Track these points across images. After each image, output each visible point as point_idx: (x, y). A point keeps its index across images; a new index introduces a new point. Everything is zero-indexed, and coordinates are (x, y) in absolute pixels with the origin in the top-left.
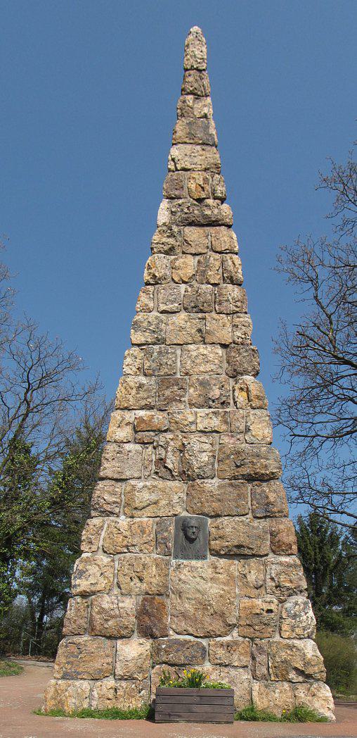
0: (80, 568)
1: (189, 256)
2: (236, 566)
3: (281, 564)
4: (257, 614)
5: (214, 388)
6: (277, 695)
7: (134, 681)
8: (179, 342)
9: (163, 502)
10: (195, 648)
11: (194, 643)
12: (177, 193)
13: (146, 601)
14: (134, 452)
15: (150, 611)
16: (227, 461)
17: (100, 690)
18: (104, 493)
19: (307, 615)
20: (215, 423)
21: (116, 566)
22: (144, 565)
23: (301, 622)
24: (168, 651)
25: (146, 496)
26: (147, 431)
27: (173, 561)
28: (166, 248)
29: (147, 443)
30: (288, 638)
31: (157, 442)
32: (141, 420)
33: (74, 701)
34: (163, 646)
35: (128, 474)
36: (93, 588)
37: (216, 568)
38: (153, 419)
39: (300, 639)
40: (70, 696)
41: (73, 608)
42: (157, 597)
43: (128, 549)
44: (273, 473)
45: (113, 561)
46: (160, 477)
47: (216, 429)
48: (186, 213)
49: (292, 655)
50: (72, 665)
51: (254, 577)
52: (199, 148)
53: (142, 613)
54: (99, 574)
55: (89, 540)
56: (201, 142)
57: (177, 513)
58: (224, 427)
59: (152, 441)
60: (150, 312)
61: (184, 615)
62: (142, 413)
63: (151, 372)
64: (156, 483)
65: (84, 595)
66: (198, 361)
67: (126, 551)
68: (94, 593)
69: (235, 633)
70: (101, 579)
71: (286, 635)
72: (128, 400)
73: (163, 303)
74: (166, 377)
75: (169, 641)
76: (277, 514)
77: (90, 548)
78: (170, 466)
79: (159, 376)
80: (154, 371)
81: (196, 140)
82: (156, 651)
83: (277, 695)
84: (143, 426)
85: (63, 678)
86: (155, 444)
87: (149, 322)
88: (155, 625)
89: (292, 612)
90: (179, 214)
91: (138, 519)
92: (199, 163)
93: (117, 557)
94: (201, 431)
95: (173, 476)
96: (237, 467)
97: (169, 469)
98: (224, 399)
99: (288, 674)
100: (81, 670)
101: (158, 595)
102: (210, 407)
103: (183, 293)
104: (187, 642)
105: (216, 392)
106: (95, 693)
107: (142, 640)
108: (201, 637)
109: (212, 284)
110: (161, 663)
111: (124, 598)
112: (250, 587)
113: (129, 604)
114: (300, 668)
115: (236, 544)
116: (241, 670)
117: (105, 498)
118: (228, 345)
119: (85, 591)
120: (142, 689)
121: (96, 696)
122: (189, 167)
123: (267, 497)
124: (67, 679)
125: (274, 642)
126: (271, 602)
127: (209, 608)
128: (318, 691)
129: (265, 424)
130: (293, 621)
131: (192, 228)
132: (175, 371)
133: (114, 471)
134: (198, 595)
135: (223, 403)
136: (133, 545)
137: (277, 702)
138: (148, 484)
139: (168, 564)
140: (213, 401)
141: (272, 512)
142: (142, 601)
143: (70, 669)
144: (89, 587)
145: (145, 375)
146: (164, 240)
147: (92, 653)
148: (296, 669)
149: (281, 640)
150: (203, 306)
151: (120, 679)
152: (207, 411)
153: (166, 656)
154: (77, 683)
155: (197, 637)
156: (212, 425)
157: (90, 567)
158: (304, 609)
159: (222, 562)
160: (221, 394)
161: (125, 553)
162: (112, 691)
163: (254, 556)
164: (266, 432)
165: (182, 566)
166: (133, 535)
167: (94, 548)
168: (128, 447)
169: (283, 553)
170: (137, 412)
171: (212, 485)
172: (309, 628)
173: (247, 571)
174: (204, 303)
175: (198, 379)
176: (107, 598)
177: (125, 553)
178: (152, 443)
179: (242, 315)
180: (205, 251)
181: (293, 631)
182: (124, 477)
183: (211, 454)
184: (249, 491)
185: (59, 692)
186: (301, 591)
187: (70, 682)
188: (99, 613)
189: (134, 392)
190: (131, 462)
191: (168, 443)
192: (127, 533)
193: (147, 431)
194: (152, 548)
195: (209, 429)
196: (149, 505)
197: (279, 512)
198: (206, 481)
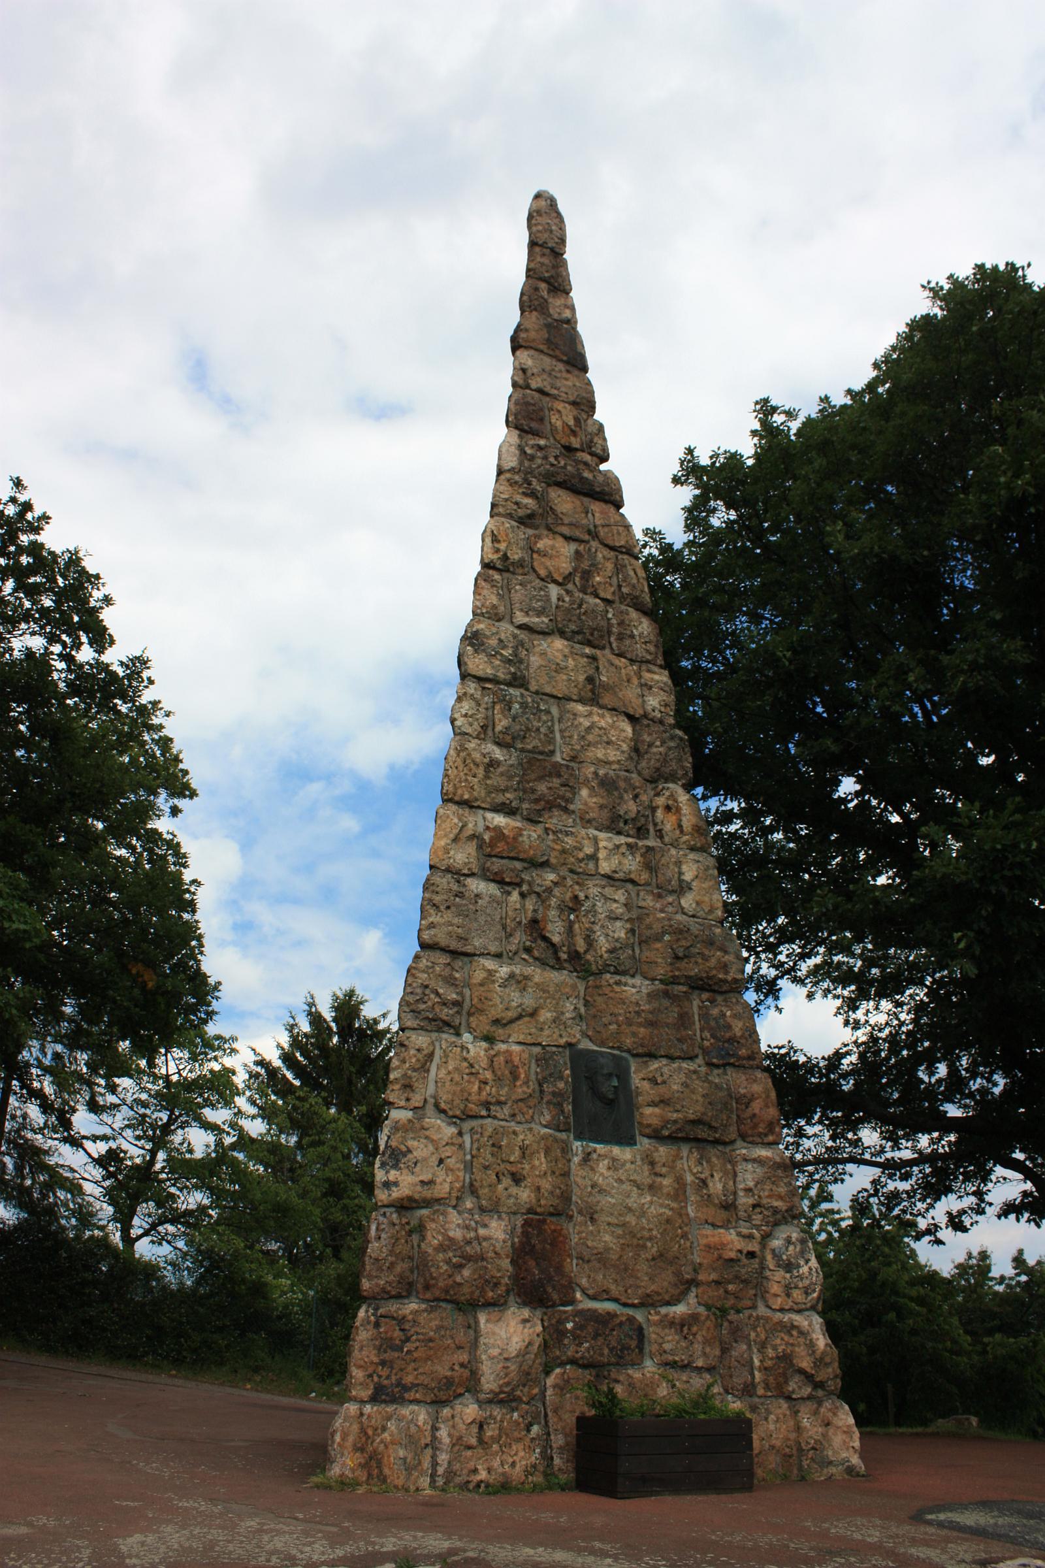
1: (561, 539)
2: (688, 1162)
3: (758, 1161)
4: (732, 1260)
7: (514, 1404)
8: (555, 693)
9: (546, 1015)
10: (626, 1328)
11: (624, 1319)
12: (534, 425)
13: (530, 1225)
14: (487, 899)
15: (538, 1247)
16: (658, 945)
17: (453, 1427)
19: (810, 1264)
20: (631, 864)
21: (468, 1145)
22: (523, 1149)
23: (801, 1277)
24: (578, 1336)
26: (508, 858)
27: (577, 1145)
28: (521, 512)
29: (509, 884)
30: (781, 1310)
31: (530, 884)
33: (401, 1453)
34: (569, 1325)
36: (427, 1193)
38: (521, 835)
40: (393, 1443)
41: (383, 1236)
42: (549, 1219)
43: (488, 1110)
45: (460, 1134)
46: (536, 959)
47: (633, 876)
48: (552, 465)
49: (792, 1345)
50: (392, 1368)
51: (719, 1186)
52: (560, 366)
53: (523, 1252)
54: (434, 1160)
55: (406, 1082)
56: (565, 358)
58: (644, 876)
59: (518, 880)
60: (499, 620)
61: (601, 1258)
62: (499, 820)
63: (508, 739)
64: (529, 970)
65: (405, 1206)
66: (590, 737)
67: (484, 1113)
68: (427, 1203)
69: (692, 1298)
70: (441, 1175)
71: (777, 1303)
72: (472, 788)
73: (521, 610)
74: (541, 757)
77: (408, 1100)
79: (522, 750)
80: (514, 738)
81: (558, 353)
82: (554, 1335)
84: (501, 847)
85: (374, 1399)
86: (525, 888)
87: (501, 641)
88: (550, 1279)
89: (784, 1257)
90: (539, 461)
91: (503, 1047)
92: (563, 389)
93: (467, 1126)
95: (558, 959)
96: (677, 958)
97: (553, 945)
99: (786, 1382)
101: (551, 1214)
102: (619, 833)
103: (554, 599)
104: (611, 1315)
105: (630, 807)
106: (443, 1433)
107: (526, 1313)
108: (633, 1306)
109: (603, 600)
110: (562, 1364)
111: (486, 1219)
112: (715, 1205)
113: (497, 1231)
114: (809, 1370)
115: (692, 1117)
117: (441, 991)
120: (531, 1424)
121: (447, 1440)
122: (548, 389)
124: (385, 1402)
125: (758, 1318)
126: (750, 1237)
127: (649, 1244)
128: (835, 1414)
130: (788, 1275)
131: (561, 492)
132: (551, 748)
133: (449, 934)
134: (631, 1219)
136: (499, 1103)
139: (566, 1149)
140: (626, 822)
141: (740, 1058)
142: (523, 1226)
143: (388, 1377)
144: (419, 1188)
145: (498, 744)
146: (518, 498)
147: (431, 1340)
148: (801, 1371)
149: (769, 1313)
150: (592, 634)
151: (490, 1401)
153: (572, 1348)
154: (406, 1411)
155: (625, 1305)
156: (626, 868)
157: (416, 1143)
158: (802, 1252)
159: (663, 1152)
161: (482, 1117)
162: (475, 1429)
163: (717, 1142)
165: (595, 1156)
166: (498, 1079)
167: (417, 1100)
169: (759, 1140)
170: (489, 815)
172: (814, 1291)
173: (706, 1174)
174: (594, 629)
175: (596, 774)
176: (454, 1217)
177: (482, 1117)
178: (519, 885)
180: (587, 537)
181: (788, 1295)
182: (469, 949)
183: (628, 926)
184: (695, 1009)
185: (370, 1432)
187: (390, 1409)
188: (441, 1248)
189: (481, 772)
190: (482, 919)
192: (488, 1075)
193: (508, 858)
194: (531, 1111)
195: (620, 875)
196: (520, 1017)
198: (623, 979)
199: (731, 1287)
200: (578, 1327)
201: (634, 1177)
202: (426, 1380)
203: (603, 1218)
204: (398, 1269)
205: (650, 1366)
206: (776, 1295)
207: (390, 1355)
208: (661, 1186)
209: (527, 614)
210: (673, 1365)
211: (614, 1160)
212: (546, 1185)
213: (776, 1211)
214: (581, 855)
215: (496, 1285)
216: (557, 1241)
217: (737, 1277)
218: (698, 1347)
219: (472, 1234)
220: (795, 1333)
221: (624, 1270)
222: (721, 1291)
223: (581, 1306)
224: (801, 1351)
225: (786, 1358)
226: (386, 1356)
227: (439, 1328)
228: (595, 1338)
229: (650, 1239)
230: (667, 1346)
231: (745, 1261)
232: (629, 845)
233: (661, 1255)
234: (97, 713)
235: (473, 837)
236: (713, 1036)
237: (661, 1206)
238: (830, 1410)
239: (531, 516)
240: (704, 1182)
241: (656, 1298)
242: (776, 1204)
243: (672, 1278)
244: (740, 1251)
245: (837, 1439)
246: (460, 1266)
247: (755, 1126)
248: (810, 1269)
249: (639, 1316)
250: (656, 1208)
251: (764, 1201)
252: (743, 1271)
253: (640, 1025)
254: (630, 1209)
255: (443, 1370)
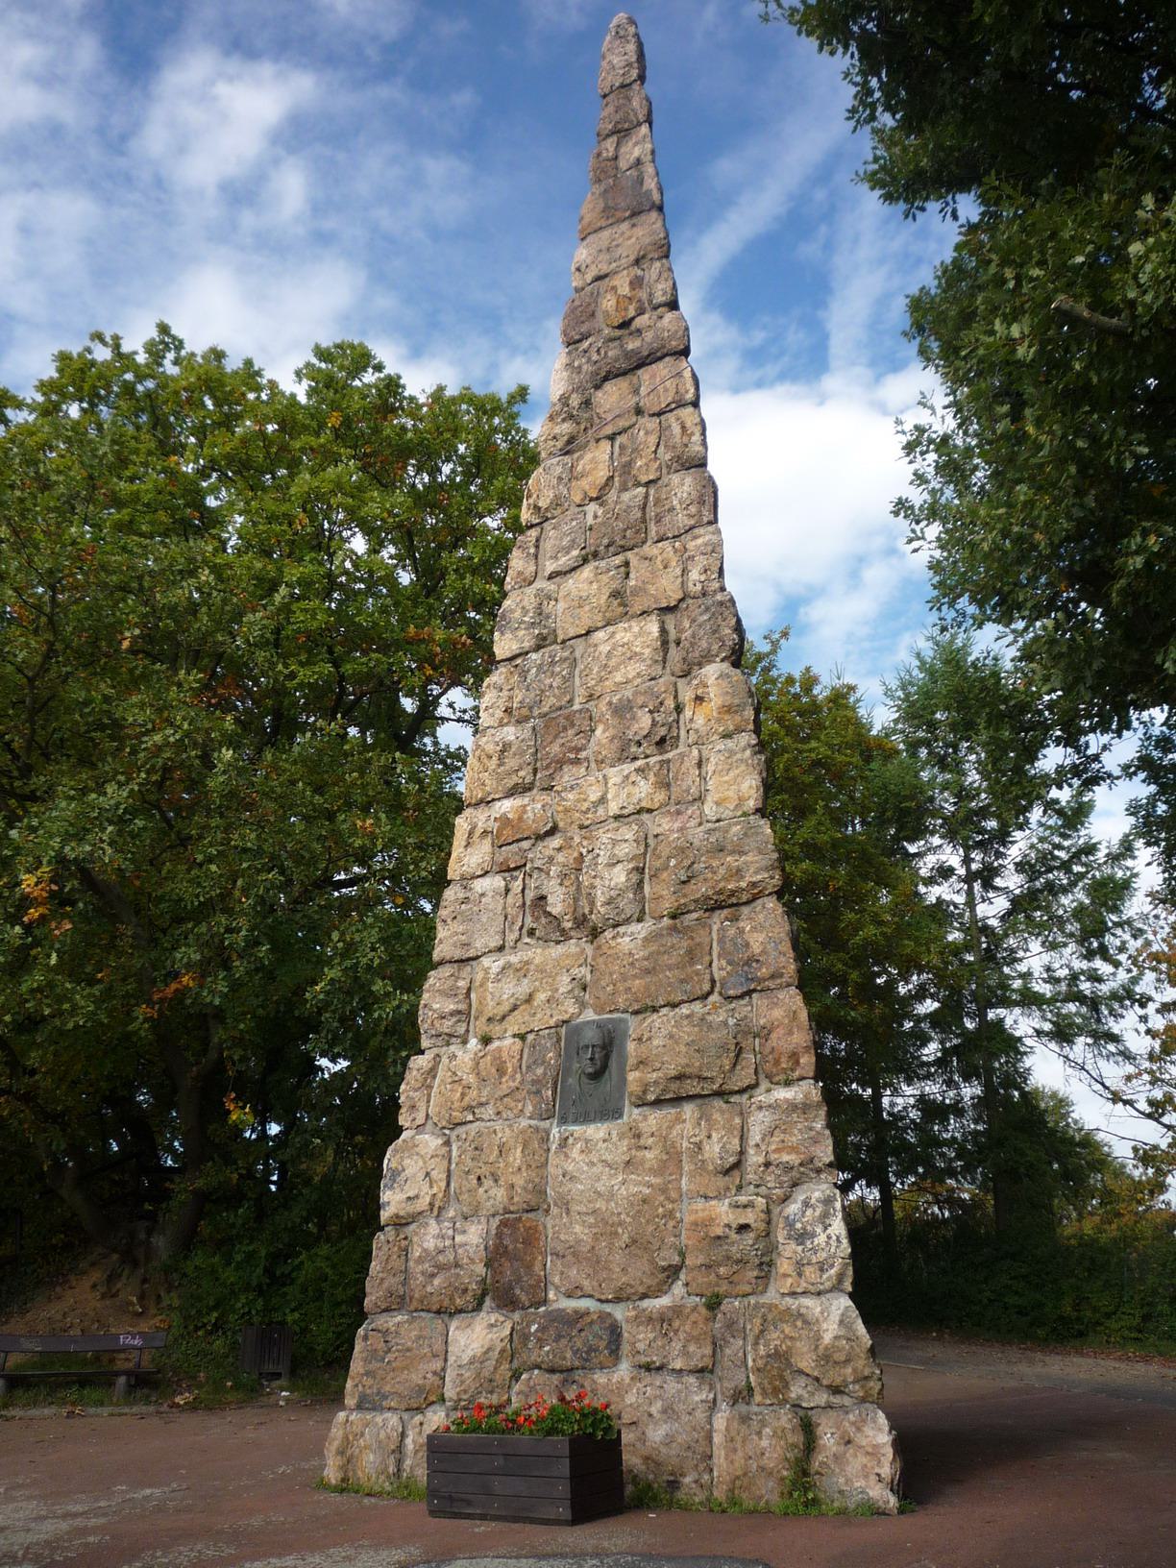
0: (393, 1165)
5: (640, 713)
6: (765, 1443)
9: (541, 997)
10: (596, 1328)
18: (435, 1000)
20: (644, 790)
25: (510, 990)
30: (793, 1294)
32: (504, 821)
35: (479, 944)
36: (411, 1208)
37: (638, 1136)
39: (819, 1294)
42: (525, 1216)
44: (754, 884)
52: (625, 226)
53: (496, 1255)
57: (566, 1017)
58: (660, 797)
62: (506, 806)
63: (525, 712)
67: (470, 1118)
69: (678, 1289)
75: (548, 1313)
76: (770, 984)
78: (555, 911)
81: (619, 214)
83: (765, 1443)
94: (617, 817)
98: (663, 731)
100: (387, 1388)
102: (635, 759)
104: (580, 1315)
108: (607, 1301)
112: (708, 1172)
113: (474, 1236)
115: (673, 1073)
116: (692, 1379)
118: (676, 607)
119: (397, 1216)
123: (747, 945)
128: (859, 1429)
129: (743, 767)
134: (600, 1204)
135: (662, 742)
136: (481, 1104)
137: (765, 1462)
138: (514, 959)
140: (639, 744)
147: (409, 1350)
152: (628, 768)
158: (825, 1215)
160: (654, 724)
164: (745, 786)
168: (480, 885)
171: (631, 939)
175: (610, 703)
176: (433, 1228)
179: (702, 531)
181: (800, 1275)
182: (472, 953)
186: (819, 1171)
191: (551, 859)
196: (515, 1008)
197: (773, 977)
199: (722, 1270)
200: (542, 1329)
201: (608, 1157)
202: (400, 1388)
203: (575, 1208)
204: (386, 1285)
205: (624, 1370)
206: (786, 1276)
207: (374, 1365)
208: (642, 1162)
209: (556, 558)
210: (648, 1368)
211: (587, 1141)
212: (519, 1181)
213: (788, 1168)
214: (586, 805)
215: (465, 1291)
216: (531, 1239)
217: (729, 1258)
218: (677, 1345)
219: (448, 1243)
220: (799, 1323)
221: (595, 1262)
222: (712, 1277)
223: (555, 1306)
224: (802, 1346)
225: (781, 1357)
226: (371, 1367)
227: (419, 1337)
228: (557, 1340)
229: (620, 1224)
230: (641, 1346)
231: (734, 1236)
232: (637, 770)
233: (634, 1242)
234: (1128, 434)
235: (485, 832)
236: (729, 963)
237: (639, 1183)
238: (853, 1424)
239: (571, 440)
240: (699, 1146)
241: (630, 1290)
242: (786, 1158)
243: (647, 1268)
244: (728, 1226)
245: (856, 1462)
246: (433, 1276)
247: (777, 1062)
248: (829, 1237)
249: (619, 1312)
250: (633, 1187)
251: (773, 1157)
252: (734, 1249)
253: (635, 977)
254: (599, 1194)
255: (416, 1378)
